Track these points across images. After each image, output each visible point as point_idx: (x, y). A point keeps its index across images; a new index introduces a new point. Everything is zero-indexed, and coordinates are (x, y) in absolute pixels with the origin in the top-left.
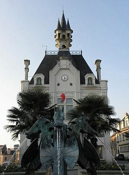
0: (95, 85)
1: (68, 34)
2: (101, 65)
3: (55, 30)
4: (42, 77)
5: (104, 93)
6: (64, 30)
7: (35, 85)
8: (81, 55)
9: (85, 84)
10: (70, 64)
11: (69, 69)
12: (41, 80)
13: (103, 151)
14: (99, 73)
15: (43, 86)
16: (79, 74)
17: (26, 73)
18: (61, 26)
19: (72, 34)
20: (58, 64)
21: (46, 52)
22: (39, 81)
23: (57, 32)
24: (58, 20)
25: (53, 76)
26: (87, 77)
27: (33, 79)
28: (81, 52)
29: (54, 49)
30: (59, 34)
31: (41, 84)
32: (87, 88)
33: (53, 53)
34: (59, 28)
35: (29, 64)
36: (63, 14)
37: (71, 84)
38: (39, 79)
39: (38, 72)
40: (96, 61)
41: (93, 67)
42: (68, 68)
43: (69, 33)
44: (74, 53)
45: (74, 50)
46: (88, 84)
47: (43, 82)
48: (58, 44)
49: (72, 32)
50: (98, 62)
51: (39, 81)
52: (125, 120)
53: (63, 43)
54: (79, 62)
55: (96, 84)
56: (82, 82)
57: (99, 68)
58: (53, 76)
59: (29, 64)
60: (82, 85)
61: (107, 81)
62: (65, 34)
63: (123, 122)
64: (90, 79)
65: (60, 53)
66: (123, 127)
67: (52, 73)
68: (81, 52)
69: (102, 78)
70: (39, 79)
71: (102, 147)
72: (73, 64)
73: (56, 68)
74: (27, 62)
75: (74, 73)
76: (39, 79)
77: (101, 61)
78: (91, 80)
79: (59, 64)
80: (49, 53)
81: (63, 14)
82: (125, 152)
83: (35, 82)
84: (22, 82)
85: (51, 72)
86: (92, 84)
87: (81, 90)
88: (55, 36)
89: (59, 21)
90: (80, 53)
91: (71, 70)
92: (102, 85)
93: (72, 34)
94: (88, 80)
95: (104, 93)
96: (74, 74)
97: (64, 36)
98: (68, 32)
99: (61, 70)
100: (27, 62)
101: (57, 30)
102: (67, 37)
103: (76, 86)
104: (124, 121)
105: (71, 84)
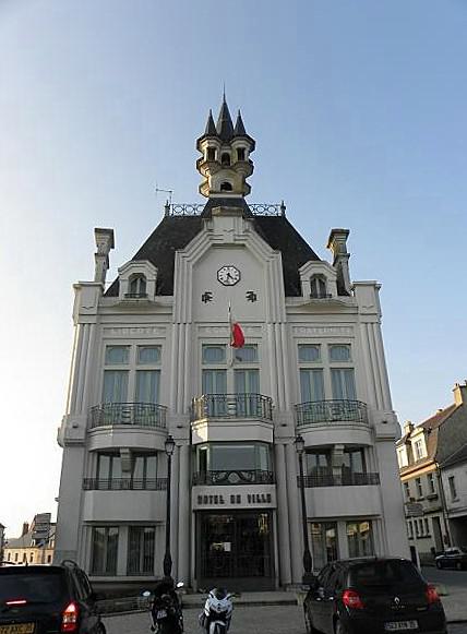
0: (335, 296)
1: (241, 152)
2: (350, 245)
3: (200, 139)
4: (150, 271)
5: (369, 325)
6: (227, 145)
7: (121, 296)
8: (283, 217)
9: (300, 295)
10: (247, 231)
11: (244, 245)
12: (143, 284)
13: (375, 534)
14: (344, 271)
15: (152, 299)
16: (279, 272)
17: (97, 269)
18: (219, 132)
19: (252, 156)
20: (205, 230)
21: (168, 207)
22: (138, 286)
23: (205, 146)
24: (209, 115)
25: (188, 268)
26: (306, 272)
27: (116, 283)
28: (283, 208)
29: (191, 195)
30: (211, 151)
31: (145, 295)
32: (308, 309)
33: (189, 211)
34: (211, 133)
35: (113, 247)
36: (225, 104)
37: (252, 297)
38: (138, 280)
39: (140, 256)
40: (334, 233)
41: (326, 254)
42: (241, 242)
43: (241, 146)
44: (260, 212)
45: (262, 196)
46: (313, 295)
47: (151, 288)
48: (207, 182)
49: (253, 149)
50: (338, 235)
51: (138, 286)
52: (413, 441)
53: (222, 177)
54: (277, 231)
55: (339, 295)
56: (292, 287)
57: (341, 256)
58: (188, 268)
59: (113, 247)
60: (290, 299)
61: (377, 288)
62: (229, 152)
63: (404, 447)
64: (318, 280)
65: (212, 203)
66: (406, 463)
67: (183, 261)
68: (283, 208)
69: (355, 275)
70: (139, 282)
71: (370, 522)
72: (256, 230)
73: (200, 243)
74: (106, 237)
75: (261, 260)
76: (139, 282)
77: (347, 233)
78: (323, 284)
79: (211, 230)
80: (178, 212)
81: (225, 104)
82: (422, 537)
83: (124, 288)
84: (79, 287)
85: (181, 255)
86: (324, 295)
87: (288, 314)
88: (198, 143)
89: (211, 117)
90: (280, 212)
91: (252, 250)
92: (360, 298)
93: (252, 156)
94: (313, 284)
95: (369, 325)
96: (265, 265)
97: (226, 158)
98: (239, 144)
99: (217, 251)
100: (106, 237)
101: (203, 137)
102: (235, 158)
103: (269, 278)
104: (408, 443)
105: (252, 297)
